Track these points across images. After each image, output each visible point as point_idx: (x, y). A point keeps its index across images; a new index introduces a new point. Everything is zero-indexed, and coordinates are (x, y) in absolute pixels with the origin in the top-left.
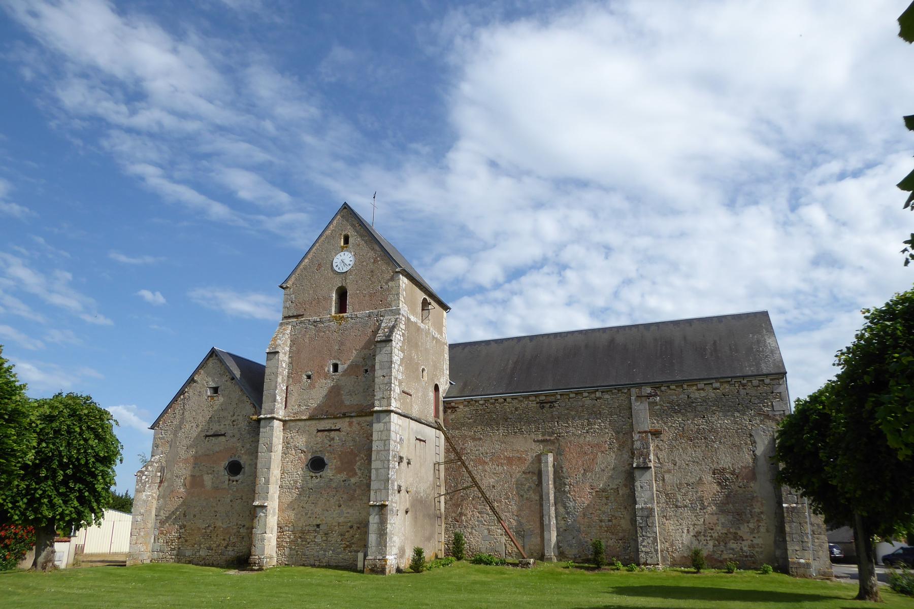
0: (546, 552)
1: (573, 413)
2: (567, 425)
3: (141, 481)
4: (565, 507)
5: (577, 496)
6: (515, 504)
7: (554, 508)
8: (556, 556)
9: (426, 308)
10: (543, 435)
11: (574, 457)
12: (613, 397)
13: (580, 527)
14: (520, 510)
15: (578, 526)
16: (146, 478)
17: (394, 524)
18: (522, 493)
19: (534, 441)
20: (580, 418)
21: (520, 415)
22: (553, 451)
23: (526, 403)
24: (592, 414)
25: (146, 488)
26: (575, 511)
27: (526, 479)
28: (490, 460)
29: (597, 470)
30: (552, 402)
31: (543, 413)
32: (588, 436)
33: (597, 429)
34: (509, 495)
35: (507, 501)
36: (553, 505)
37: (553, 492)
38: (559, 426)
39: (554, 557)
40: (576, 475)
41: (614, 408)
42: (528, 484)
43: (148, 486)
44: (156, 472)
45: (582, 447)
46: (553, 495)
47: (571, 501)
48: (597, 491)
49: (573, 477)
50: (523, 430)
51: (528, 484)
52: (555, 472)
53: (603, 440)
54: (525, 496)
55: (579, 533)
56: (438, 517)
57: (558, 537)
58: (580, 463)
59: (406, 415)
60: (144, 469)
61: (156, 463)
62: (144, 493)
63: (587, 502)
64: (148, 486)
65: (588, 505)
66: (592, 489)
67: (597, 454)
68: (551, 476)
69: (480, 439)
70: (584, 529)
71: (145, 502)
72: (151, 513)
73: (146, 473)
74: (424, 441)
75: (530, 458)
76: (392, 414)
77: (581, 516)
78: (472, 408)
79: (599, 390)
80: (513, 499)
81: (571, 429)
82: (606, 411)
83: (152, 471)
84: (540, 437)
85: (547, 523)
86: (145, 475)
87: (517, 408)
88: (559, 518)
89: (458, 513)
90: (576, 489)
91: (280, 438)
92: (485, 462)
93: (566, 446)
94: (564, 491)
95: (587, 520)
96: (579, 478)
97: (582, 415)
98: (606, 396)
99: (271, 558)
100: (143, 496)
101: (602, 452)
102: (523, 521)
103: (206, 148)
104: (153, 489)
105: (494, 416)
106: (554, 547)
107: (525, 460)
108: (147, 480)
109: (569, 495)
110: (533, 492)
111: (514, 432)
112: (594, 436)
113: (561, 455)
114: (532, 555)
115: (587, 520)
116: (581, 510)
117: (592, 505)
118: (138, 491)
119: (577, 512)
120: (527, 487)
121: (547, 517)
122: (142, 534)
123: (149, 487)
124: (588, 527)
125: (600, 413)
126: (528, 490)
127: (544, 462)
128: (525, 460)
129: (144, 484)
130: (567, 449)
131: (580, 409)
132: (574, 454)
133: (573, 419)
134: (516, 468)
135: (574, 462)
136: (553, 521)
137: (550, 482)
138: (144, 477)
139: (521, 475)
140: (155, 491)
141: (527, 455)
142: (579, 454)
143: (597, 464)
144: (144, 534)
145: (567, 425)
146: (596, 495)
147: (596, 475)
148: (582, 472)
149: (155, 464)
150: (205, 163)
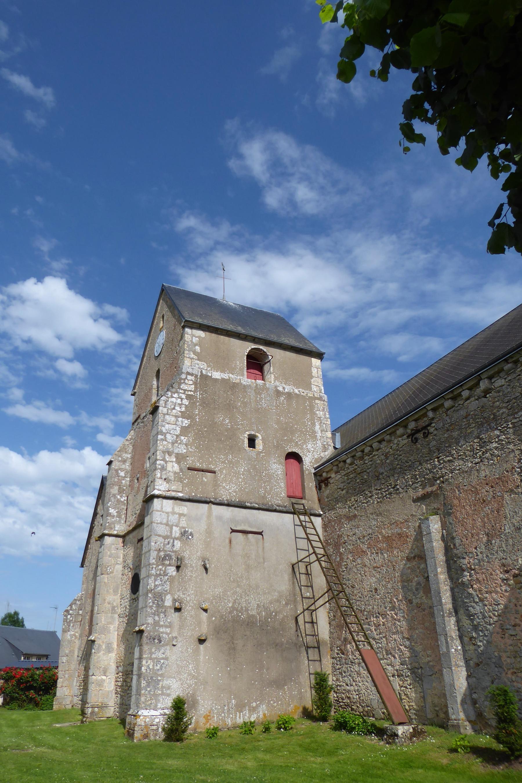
0: (450, 711)
1: (455, 434)
2: (451, 458)
3: (66, 621)
4: (470, 616)
5: (484, 589)
6: (403, 617)
7: (453, 620)
8: (470, 722)
9: (267, 361)
10: (424, 487)
11: (467, 514)
12: (509, 378)
13: (500, 657)
14: (411, 628)
15: (496, 654)
16: (70, 617)
17: (166, 659)
18: (410, 596)
19: (414, 501)
20: (466, 437)
21: (391, 463)
22: (439, 512)
23: (396, 442)
24: (482, 424)
25: (70, 627)
26: (486, 623)
27: (412, 569)
28: (368, 548)
29: (507, 531)
30: (425, 427)
31: (418, 449)
32: (483, 468)
33: (496, 448)
34: (395, 602)
35: (393, 612)
36: (450, 613)
37: (448, 588)
38: (441, 464)
39: (467, 723)
40: (476, 548)
41: (515, 398)
42: (416, 579)
43: (72, 625)
44: (79, 610)
45: (477, 492)
46: (448, 594)
47: (476, 603)
48: (515, 576)
49: (472, 553)
50: (398, 487)
51: (416, 579)
52: (447, 550)
53: (508, 466)
54: (415, 601)
55: (501, 670)
56: (308, 648)
57: (470, 681)
58: (479, 523)
59: (200, 499)
60: (69, 608)
61: (79, 601)
62: (69, 633)
63: (503, 601)
64: (72, 625)
65: (506, 607)
66: (507, 572)
67: (502, 497)
68: (441, 557)
69: (355, 516)
70: (509, 660)
71: (70, 642)
72: (74, 653)
73: (71, 612)
74: (260, 533)
75: (412, 530)
76: (156, 500)
77: (498, 633)
78: (343, 473)
79: (483, 377)
80: (400, 609)
81: (456, 463)
82: (504, 410)
83: (76, 610)
84: (421, 492)
85: (445, 650)
86: (70, 614)
87: (387, 454)
88: (466, 639)
89: (343, 639)
90: (481, 577)
91: (119, 558)
92: (363, 551)
93: (454, 496)
94: (463, 583)
95: (509, 642)
96: (481, 553)
97: (469, 431)
98: (499, 382)
99: (103, 707)
100: (68, 636)
101: (511, 491)
102: (418, 648)
103: (355, 332)
104: (75, 629)
105: (365, 477)
106: (463, 702)
107: (407, 537)
108: (71, 619)
109: (471, 591)
110: (424, 593)
111: (389, 494)
112: (491, 465)
113: (449, 514)
114: (437, 716)
115: (509, 642)
116: (495, 619)
117: (512, 605)
118: (64, 631)
119: (490, 625)
120: (414, 584)
121: (443, 638)
122: (67, 676)
123: (73, 626)
124: (515, 657)
125: (495, 418)
126: (417, 589)
127: (425, 533)
128: (407, 537)
129: (69, 624)
130: (456, 502)
131: (464, 423)
132: (468, 508)
133: (457, 443)
134: (398, 553)
135: (469, 521)
136: (456, 647)
137: (439, 570)
138: (69, 616)
139: (405, 564)
140: (77, 630)
141: (408, 528)
142: (475, 505)
143: (506, 517)
144: (68, 677)
145: (451, 458)
146: (516, 583)
147: (507, 541)
148: (485, 539)
149: (78, 602)
150: (362, 343)
